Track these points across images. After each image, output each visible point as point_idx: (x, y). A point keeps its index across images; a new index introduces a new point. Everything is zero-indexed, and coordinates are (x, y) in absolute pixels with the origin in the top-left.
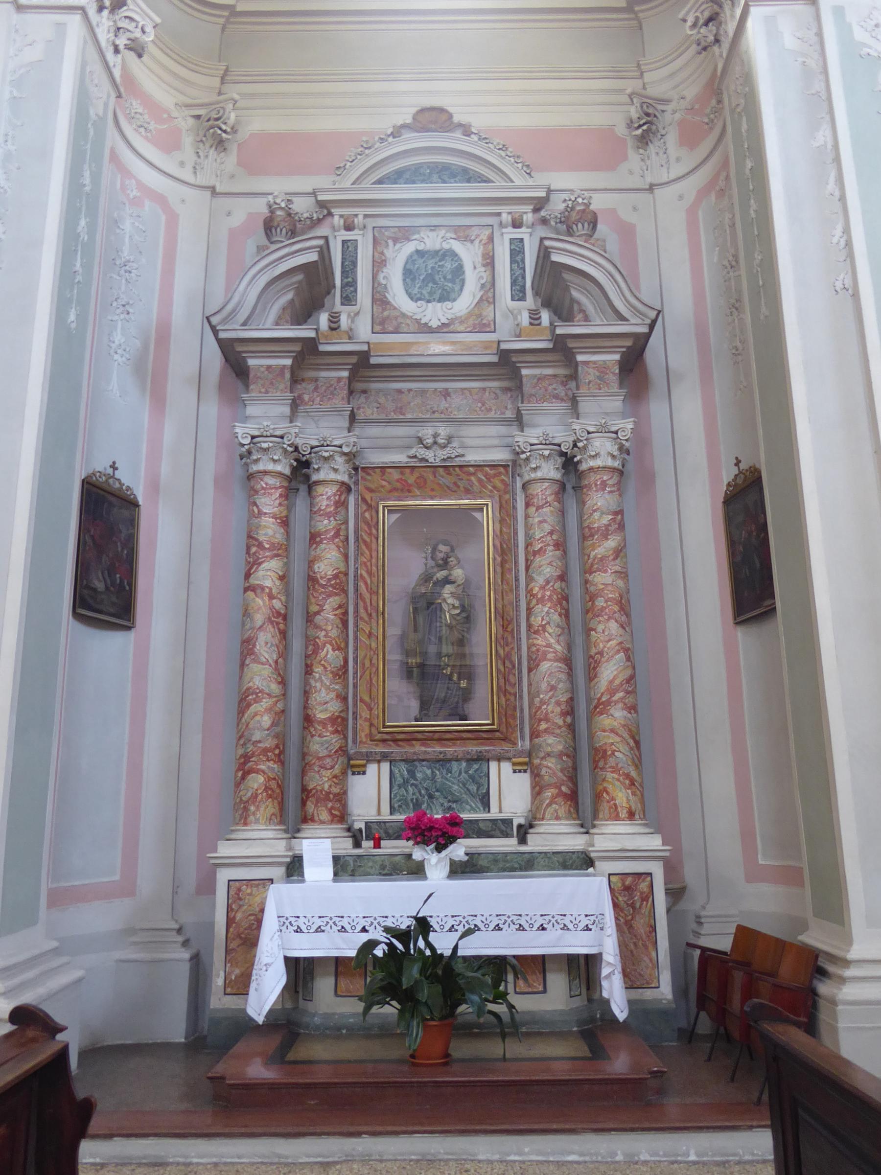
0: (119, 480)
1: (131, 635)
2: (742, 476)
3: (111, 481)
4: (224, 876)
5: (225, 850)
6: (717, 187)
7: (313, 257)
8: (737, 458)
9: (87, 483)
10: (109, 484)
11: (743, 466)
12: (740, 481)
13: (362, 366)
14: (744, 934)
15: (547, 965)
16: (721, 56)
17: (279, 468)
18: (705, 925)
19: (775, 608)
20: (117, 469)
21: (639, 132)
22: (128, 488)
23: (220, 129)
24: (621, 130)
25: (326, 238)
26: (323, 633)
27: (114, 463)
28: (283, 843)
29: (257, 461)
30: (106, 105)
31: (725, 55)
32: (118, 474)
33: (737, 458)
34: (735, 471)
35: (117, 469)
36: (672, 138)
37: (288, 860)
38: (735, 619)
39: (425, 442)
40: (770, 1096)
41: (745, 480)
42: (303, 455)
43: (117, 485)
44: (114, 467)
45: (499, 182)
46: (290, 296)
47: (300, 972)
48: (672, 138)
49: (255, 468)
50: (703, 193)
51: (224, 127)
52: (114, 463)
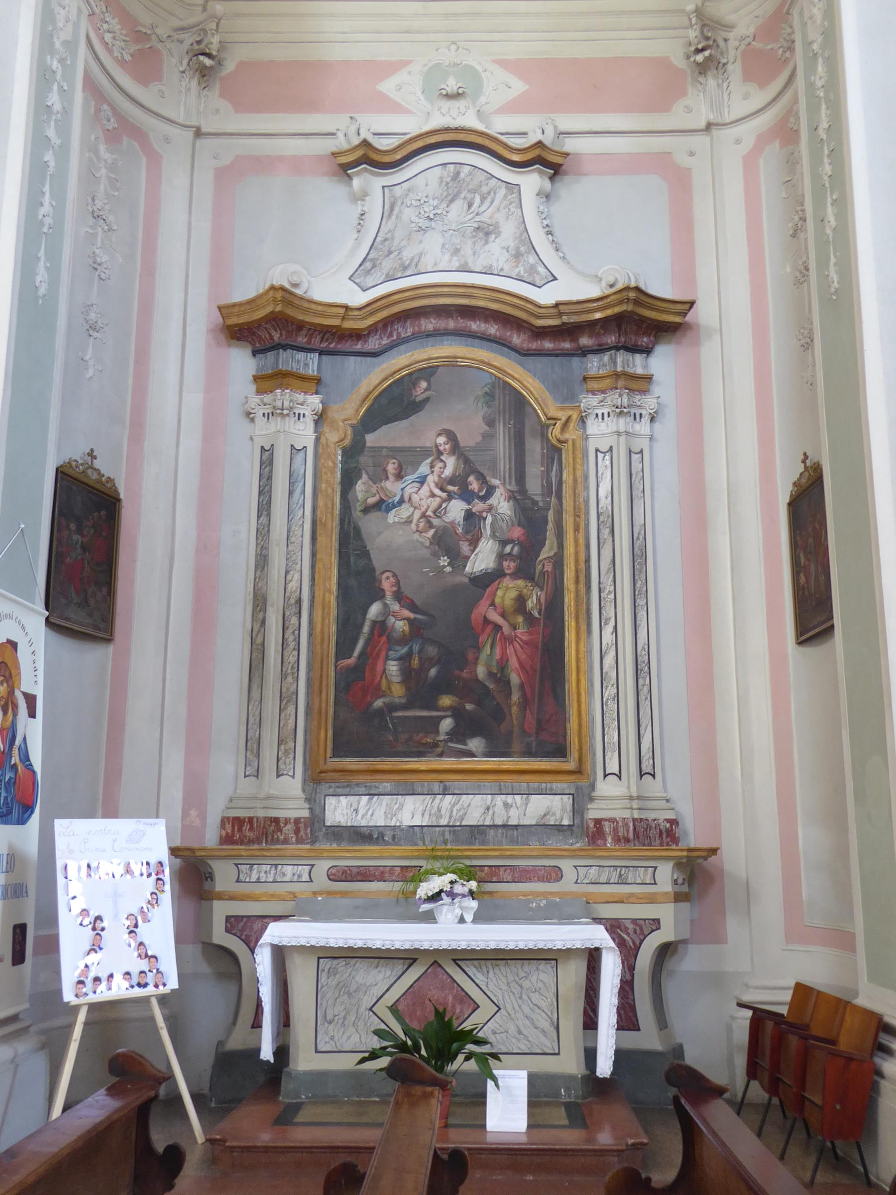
0: (98, 471)
1: (111, 648)
3: (90, 472)
6: (785, 132)
8: (805, 454)
9: (62, 472)
10: (86, 476)
12: (804, 481)
14: (802, 991)
15: (862, 1147)
19: (832, 627)
20: (95, 458)
21: (700, 58)
22: (109, 480)
24: (679, 61)
26: (790, 31)
27: (92, 450)
30: (76, 26)
32: (97, 464)
33: (805, 454)
35: (95, 458)
36: (735, 70)
38: (797, 638)
40: (686, 1099)
41: (809, 479)
43: (95, 476)
44: (91, 454)
48: (735, 70)
50: (762, 140)
52: (92, 450)
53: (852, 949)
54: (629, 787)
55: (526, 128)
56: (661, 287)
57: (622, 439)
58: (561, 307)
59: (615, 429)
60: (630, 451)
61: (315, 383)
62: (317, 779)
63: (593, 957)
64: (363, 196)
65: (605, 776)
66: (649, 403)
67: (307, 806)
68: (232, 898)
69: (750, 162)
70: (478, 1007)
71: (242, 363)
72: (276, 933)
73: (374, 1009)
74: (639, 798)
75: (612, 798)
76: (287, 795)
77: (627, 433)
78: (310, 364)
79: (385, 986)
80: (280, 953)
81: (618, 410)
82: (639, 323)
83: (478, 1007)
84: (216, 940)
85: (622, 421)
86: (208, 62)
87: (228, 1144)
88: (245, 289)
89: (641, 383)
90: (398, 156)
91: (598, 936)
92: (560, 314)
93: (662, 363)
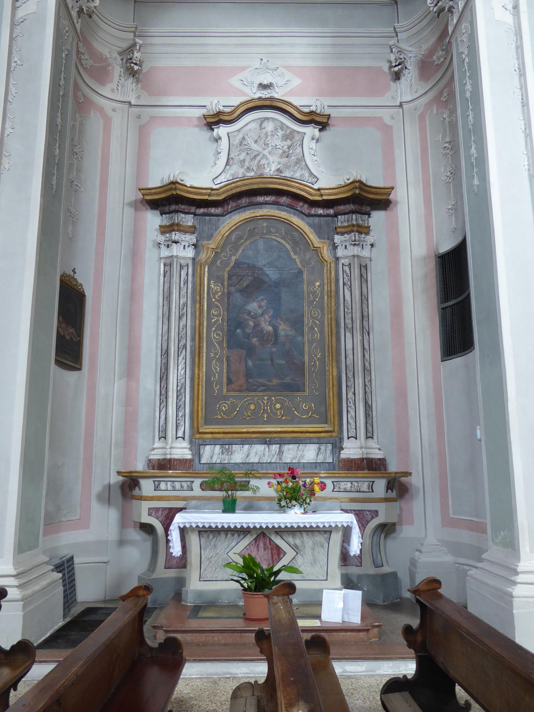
50: (429, 105)
51: (135, 62)
53: (484, 532)
54: (361, 442)
55: (304, 101)
56: (375, 180)
57: (356, 259)
58: (322, 191)
59: (352, 254)
60: (361, 265)
61: (192, 230)
62: (197, 441)
63: (347, 531)
64: (217, 139)
65: (349, 438)
66: (370, 239)
67: (190, 452)
68: (152, 499)
69: (422, 118)
70: (286, 553)
71: (154, 220)
72: (179, 519)
73: (325, 579)
74: (366, 448)
75: (351, 450)
76: (181, 450)
77: (358, 256)
78: (188, 220)
79: (236, 550)
80: (183, 531)
81: (353, 243)
82: (364, 201)
83: (286, 553)
84: (143, 521)
85: (356, 248)
86: (136, 68)
87: (12, 690)
88: (156, 179)
89: (364, 230)
90: (235, 115)
91: (350, 519)
92: (322, 195)
93: (377, 217)
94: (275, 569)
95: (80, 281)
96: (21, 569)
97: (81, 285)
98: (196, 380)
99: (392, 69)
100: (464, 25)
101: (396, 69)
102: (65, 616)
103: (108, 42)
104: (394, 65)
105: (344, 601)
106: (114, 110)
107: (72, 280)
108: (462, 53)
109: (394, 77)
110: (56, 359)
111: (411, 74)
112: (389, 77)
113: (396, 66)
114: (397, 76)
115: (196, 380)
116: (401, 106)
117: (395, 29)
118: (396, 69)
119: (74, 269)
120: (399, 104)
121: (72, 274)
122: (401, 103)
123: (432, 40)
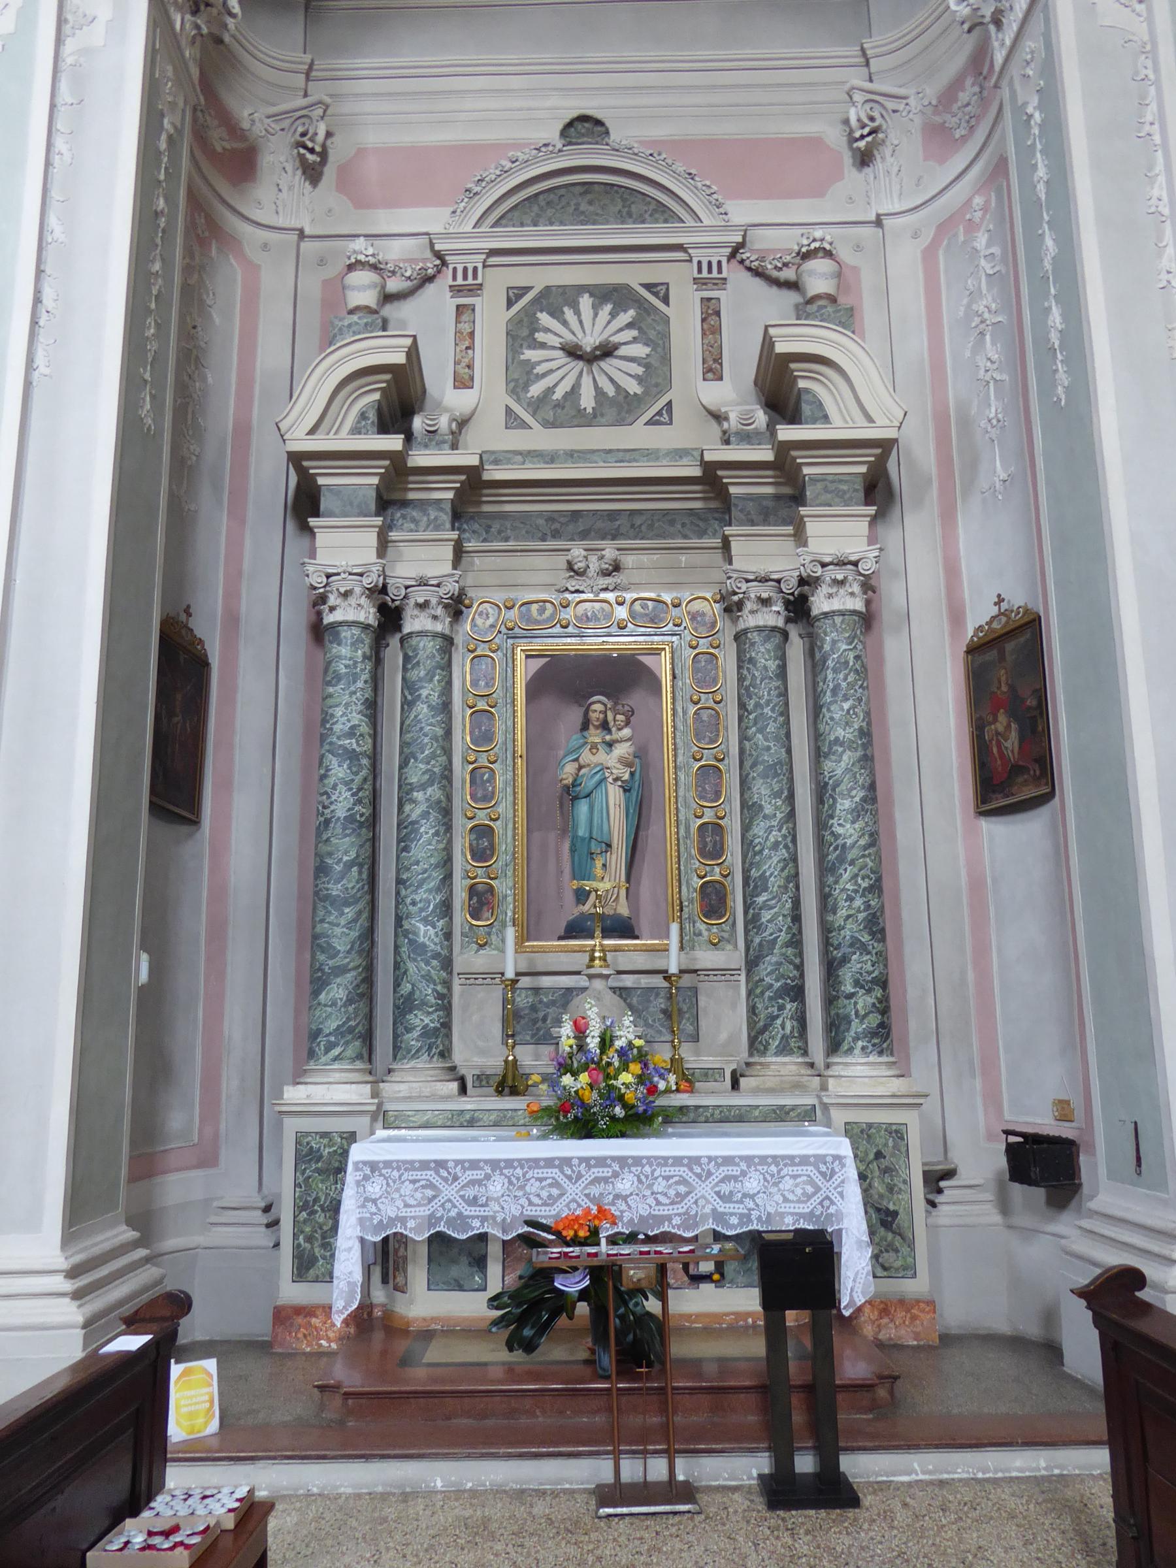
2: (1004, 619)
4: (292, 1126)
5: (294, 1094)
7: (400, 358)
8: (999, 596)
11: (1004, 606)
13: (473, 486)
16: (1003, 44)
17: (361, 617)
18: (946, 1192)
23: (305, 147)
25: (415, 337)
28: (367, 1088)
29: (332, 609)
31: (1008, 42)
33: (999, 596)
34: (995, 611)
37: (863, 469)
39: (576, 567)
41: (1004, 626)
42: (393, 600)
45: (690, 222)
46: (377, 396)
47: (387, 1256)
49: (329, 619)
51: (310, 145)
94: (1021, 1140)
95: (198, 633)
96: (78, 1258)
97: (201, 641)
98: (936, 14)
99: (855, 145)
100: (1030, 44)
101: (862, 144)
102: (84, 1350)
103: (260, 108)
104: (857, 135)
105: (918, 1347)
106: (265, 246)
107: (184, 632)
108: (1026, 104)
109: (858, 161)
110: (151, 802)
111: (903, 143)
112: (847, 159)
113: (862, 137)
114: (864, 159)
115: (936, 14)
116: (878, 222)
117: (863, 50)
118: (862, 144)
119: (189, 607)
120: (873, 218)
121: (183, 617)
122: (878, 216)
123: (960, 60)
